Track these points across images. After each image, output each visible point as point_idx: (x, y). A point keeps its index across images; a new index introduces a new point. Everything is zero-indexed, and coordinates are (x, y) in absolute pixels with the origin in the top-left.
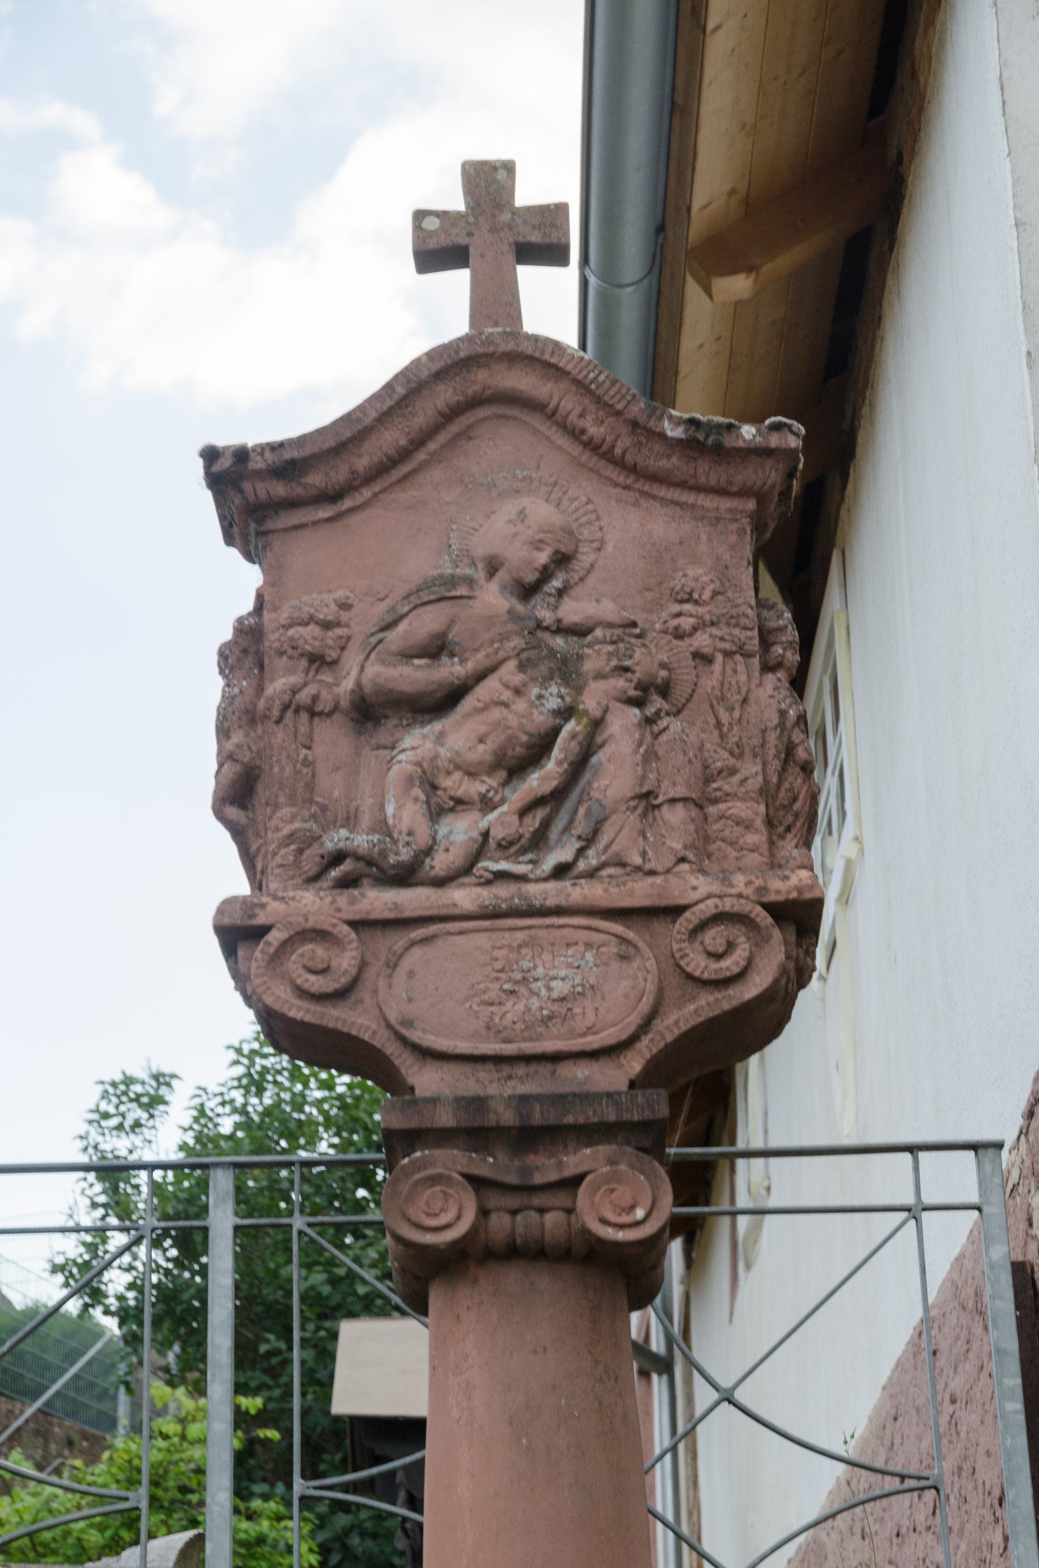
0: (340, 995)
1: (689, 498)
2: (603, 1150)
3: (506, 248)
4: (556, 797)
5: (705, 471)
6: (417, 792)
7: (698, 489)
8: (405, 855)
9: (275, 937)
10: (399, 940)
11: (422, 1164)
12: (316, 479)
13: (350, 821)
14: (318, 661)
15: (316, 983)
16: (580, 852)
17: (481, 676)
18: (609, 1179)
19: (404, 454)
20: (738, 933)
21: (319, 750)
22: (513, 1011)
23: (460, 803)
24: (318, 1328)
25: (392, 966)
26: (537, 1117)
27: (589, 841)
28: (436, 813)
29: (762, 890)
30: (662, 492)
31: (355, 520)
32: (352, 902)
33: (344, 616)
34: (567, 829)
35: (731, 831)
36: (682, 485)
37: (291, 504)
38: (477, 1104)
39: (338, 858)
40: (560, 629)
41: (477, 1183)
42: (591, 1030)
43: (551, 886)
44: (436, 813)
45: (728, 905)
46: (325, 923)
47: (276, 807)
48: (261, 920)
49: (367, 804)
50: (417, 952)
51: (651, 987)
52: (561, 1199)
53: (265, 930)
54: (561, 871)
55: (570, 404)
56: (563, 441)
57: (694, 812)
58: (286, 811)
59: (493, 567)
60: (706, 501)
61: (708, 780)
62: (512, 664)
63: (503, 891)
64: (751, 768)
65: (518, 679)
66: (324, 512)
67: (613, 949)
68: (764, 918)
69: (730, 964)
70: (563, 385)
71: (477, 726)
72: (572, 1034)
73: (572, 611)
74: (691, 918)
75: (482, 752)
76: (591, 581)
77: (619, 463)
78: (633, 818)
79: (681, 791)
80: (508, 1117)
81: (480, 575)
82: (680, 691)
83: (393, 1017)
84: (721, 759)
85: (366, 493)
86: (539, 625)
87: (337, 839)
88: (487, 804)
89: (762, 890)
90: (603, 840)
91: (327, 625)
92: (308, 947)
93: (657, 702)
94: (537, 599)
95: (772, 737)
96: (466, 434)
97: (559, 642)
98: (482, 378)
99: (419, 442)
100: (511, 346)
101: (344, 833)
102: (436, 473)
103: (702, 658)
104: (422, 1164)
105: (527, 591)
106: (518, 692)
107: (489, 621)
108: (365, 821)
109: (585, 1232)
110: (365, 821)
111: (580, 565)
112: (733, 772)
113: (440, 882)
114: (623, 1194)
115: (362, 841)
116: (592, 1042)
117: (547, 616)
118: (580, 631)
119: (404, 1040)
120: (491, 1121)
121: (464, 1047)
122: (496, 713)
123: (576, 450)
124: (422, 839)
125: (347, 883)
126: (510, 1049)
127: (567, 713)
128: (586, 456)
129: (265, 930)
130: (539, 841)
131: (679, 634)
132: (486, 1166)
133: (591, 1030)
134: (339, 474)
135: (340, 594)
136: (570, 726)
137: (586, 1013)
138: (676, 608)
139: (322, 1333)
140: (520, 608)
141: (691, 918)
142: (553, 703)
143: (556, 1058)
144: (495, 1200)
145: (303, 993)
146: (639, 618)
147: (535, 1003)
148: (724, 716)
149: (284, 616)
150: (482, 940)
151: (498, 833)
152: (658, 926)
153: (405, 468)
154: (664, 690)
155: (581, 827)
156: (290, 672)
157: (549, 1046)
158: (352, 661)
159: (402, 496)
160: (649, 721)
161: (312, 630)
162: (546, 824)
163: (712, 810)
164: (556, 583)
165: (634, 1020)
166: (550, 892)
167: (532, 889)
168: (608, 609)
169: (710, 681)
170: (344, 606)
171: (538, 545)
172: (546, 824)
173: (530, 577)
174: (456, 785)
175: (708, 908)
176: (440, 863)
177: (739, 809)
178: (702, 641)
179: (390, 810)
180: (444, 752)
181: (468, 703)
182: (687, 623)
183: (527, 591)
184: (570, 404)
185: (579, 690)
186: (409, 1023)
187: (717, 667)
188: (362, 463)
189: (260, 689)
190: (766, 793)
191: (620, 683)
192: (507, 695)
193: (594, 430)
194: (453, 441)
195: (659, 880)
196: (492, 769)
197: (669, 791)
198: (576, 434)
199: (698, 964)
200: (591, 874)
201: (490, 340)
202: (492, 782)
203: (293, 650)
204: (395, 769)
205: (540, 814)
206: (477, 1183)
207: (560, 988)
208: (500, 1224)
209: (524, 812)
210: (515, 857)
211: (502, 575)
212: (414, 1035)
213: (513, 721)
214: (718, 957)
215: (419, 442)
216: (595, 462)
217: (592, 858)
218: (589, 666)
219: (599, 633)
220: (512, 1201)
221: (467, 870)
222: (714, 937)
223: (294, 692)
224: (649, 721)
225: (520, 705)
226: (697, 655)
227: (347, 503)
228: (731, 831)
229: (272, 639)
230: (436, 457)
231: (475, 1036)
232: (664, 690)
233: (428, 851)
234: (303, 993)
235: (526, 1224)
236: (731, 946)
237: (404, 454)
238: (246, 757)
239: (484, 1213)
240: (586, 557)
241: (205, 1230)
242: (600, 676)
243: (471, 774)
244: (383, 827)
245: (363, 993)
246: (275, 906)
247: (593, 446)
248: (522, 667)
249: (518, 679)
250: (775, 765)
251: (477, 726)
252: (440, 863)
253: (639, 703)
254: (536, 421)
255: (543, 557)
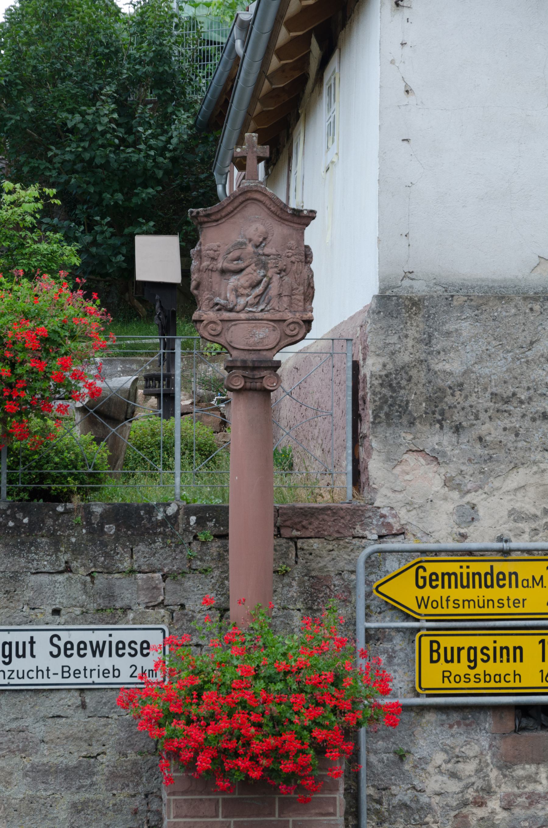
0: (218, 335)
1: (292, 225)
2: (269, 372)
3: (255, 157)
4: (261, 295)
5: (296, 219)
6: (234, 292)
7: (294, 223)
8: (231, 306)
9: (205, 322)
10: (230, 324)
11: (234, 373)
12: (213, 217)
13: (219, 295)
14: (213, 259)
15: (213, 333)
16: (266, 306)
17: (247, 267)
18: (270, 377)
19: (232, 211)
20: (296, 326)
21: (213, 279)
22: (252, 340)
23: (242, 295)
24: (78, 146)
25: (228, 330)
26: (256, 365)
27: (268, 304)
28: (237, 296)
29: (302, 317)
30: (286, 223)
31: (221, 225)
32: (221, 316)
33: (219, 249)
34: (264, 301)
35: (297, 302)
36: (291, 222)
37: (208, 222)
38: (244, 361)
39: (217, 304)
40: (264, 255)
41: (244, 377)
42: (267, 345)
43: (260, 314)
44: (237, 296)
45: (295, 320)
46: (215, 320)
47: (204, 291)
48: (202, 319)
49: (223, 293)
50: (233, 327)
51: (279, 337)
52: (260, 380)
53: (203, 321)
54: (262, 310)
55: (268, 202)
56: (266, 210)
57: (289, 298)
58: (206, 292)
59: (250, 240)
60: (296, 226)
61: (292, 290)
62: (254, 265)
63: (251, 315)
64: (301, 288)
65: (255, 268)
66: (214, 224)
67: (271, 328)
68: (302, 323)
69: (294, 333)
70: (266, 198)
71: (246, 278)
72: (263, 346)
73: (267, 251)
74: (287, 322)
75: (247, 284)
76: (271, 243)
77: (278, 216)
78: (277, 299)
79: (287, 294)
80: (250, 365)
81: (247, 242)
82: (288, 270)
83: (228, 341)
84: (295, 286)
85: (224, 220)
86: (259, 254)
87: (217, 300)
88: (248, 295)
89: (302, 317)
90: (271, 304)
91: (215, 251)
92: (211, 325)
93: (283, 273)
94: (259, 248)
95: (306, 281)
96: (245, 206)
97: (263, 257)
98: (249, 195)
99: (235, 209)
100: (256, 189)
101: (218, 298)
102: (238, 215)
103: (293, 263)
104: (234, 373)
105: (257, 247)
106: (255, 271)
107: (249, 254)
108: (223, 297)
109: (264, 387)
110: (223, 297)
111: (268, 240)
112: (297, 289)
113: (238, 312)
114: (272, 380)
115: (222, 302)
116: (267, 347)
117: (261, 252)
118: (268, 255)
119: (230, 346)
120: (247, 365)
121: (242, 347)
122: (250, 276)
123: (269, 212)
124: (235, 303)
125: (219, 310)
126: (251, 348)
127: (264, 276)
128: (270, 213)
129: (203, 321)
130: (258, 303)
131: (288, 257)
132: (247, 373)
133: (267, 345)
134: (219, 216)
135: (218, 243)
136: (265, 279)
137: (266, 341)
138: (288, 251)
139: (80, 149)
140: (256, 250)
141: (287, 322)
142: (262, 274)
143: (260, 350)
144: (248, 380)
145: (211, 335)
146: (280, 253)
147: (256, 339)
148: (297, 276)
149: (206, 248)
150: (246, 325)
151: (250, 302)
152: (281, 323)
153: (232, 214)
154: (284, 271)
155: (266, 301)
156: (207, 261)
157: (258, 348)
158: (220, 260)
159: (232, 220)
160: (281, 278)
161: (212, 252)
162: (259, 300)
163: (293, 297)
164: (263, 244)
165: (275, 343)
166: (259, 315)
167: (256, 314)
168: (273, 251)
169: (294, 268)
170: (219, 246)
171: (260, 236)
172: (259, 300)
173: (258, 244)
174: (242, 291)
175: (291, 320)
176: (238, 308)
177: (298, 297)
178: (293, 259)
179: (228, 295)
180: (239, 283)
181: (244, 272)
182: (290, 254)
183: (257, 247)
184: (268, 202)
185: (267, 271)
186: (231, 342)
187: (296, 265)
188: (223, 214)
189: (201, 264)
190: (304, 294)
191: (276, 270)
192: (252, 272)
193: (273, 209)
194: (242, 208)
195: (281, 313)
196: (249, 287)
197: (285, 293)
198: (269, 209)
199: (288, 332)
200: (268, 311)
201: (251, 187)
202: (249, 290)
203: (208, 256)
204: (229, 286)
205: (258, 298)
206: (244, 377)
207: (261, 336)
208: (248, 385)
209: (255, 298)
210: (253, 307)
211: (252, 242)
212: (232, 344)
213: (254, 278)
214: (292, 331)
215: (235, 209)
216: (272, 215)
217: (268, 308)
218: (269, 266)
219: (272, 256)
220: (251, 381)
221: (243, 309)
222: (292, 327)
223: (208, 266)
224: (281, 278)
225: (255, 274)
226: (292, 262)
227: (220, 222)
228: (297, 302)
229: (204, 253)
230: (239, 212)
231: (244, 345)
232: (284, 271)
233: (236, 305)
234: (211, 335)
235: (253, 385)
236: (295, 329)
237: (232, 211)
238: (198, 280)
239: (245, 382)
240: (270, 238)
241: (174, 353)
242: (272, 268)
243: (245, 288)
244: (226, 299)
245: (222, 335)
246: (205, 316)
247: (272, 212)
248: (256, 265)
249: (255, 268)
250: (306, 287)
251: (246, 278)
252: (238, 308)
253: (279, 274)
254: (260, 204)
255: (261, 239)
